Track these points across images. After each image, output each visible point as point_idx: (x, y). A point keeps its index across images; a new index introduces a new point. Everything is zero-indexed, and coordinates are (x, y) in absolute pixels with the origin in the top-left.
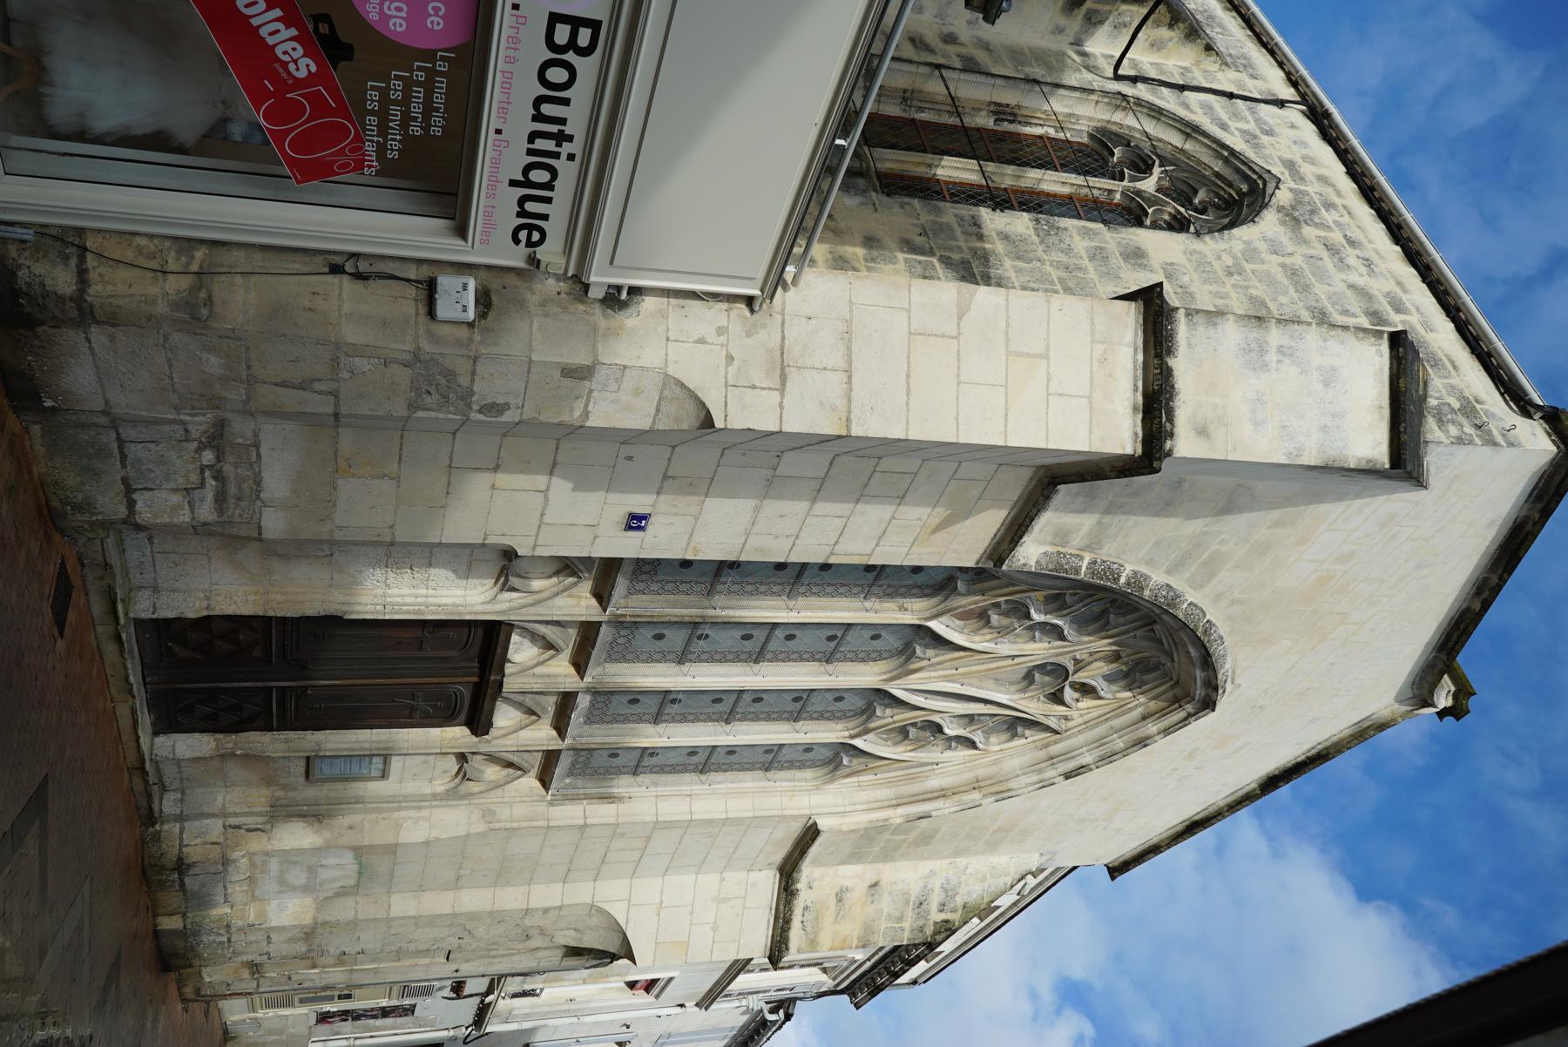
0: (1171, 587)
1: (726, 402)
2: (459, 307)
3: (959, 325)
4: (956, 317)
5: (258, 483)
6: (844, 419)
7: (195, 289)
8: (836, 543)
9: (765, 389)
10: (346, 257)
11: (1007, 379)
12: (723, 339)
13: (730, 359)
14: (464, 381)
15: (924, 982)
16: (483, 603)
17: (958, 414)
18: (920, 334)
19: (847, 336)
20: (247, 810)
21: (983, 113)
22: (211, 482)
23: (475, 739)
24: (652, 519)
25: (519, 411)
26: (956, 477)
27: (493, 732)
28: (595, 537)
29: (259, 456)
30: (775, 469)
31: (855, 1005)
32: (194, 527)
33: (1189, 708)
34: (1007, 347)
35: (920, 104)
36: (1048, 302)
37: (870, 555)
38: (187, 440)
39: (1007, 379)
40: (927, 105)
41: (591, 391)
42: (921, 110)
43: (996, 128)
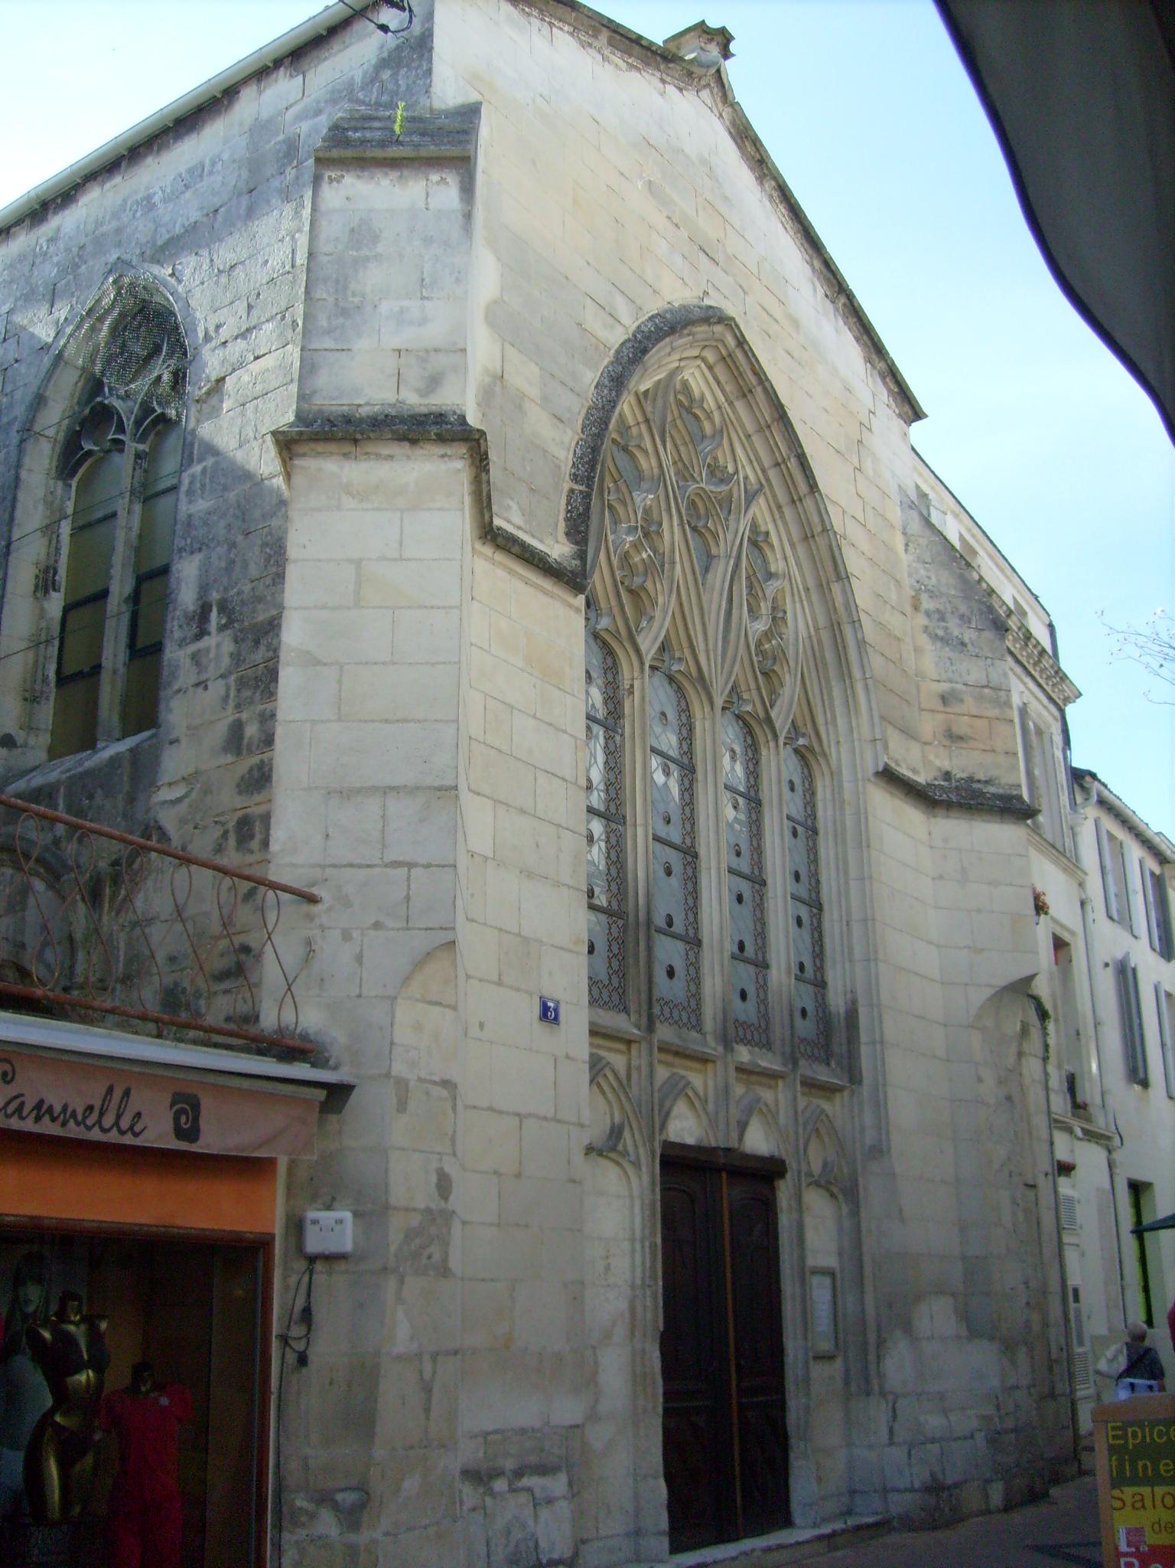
0: (598, 383)
1: (426, 929)
2: (337, 1228)
3: (325, 664)
4: (318, 668)
5: (523, 1431)
6: (439, 794)
7: (336, 1506)
8: (564, 779)
9: (409, 886)
10: (288, 1349)
11: (386, 607)
12: (355, 934)
13: (377, 925)
14: (415, 1220)
15: (1049, 615)
16: (640, 1178)
17: (427, 663)
18: (339, 709)
19: (346, 794)
21: (46, 605)
22: (526, 1481)
23: (788, 1176)
24: (546, 994)
25: (444, 1157)
26: (486, 647)
27: (784, 1157)
28: (568, 1057)
29: (496, 1432)
30: (486, 858)
31: (1077, 697)
32: (573, 1496)
33: (1067, 1550)
34: (349, 608)
35: (39, 681)
36: (296, 561)
37: (576, 738)
38: (484, 1508)
39: (386, 607)
40: (40, 673)
41: (420, 1080)
42: (45, 679)
43: (63, 590)
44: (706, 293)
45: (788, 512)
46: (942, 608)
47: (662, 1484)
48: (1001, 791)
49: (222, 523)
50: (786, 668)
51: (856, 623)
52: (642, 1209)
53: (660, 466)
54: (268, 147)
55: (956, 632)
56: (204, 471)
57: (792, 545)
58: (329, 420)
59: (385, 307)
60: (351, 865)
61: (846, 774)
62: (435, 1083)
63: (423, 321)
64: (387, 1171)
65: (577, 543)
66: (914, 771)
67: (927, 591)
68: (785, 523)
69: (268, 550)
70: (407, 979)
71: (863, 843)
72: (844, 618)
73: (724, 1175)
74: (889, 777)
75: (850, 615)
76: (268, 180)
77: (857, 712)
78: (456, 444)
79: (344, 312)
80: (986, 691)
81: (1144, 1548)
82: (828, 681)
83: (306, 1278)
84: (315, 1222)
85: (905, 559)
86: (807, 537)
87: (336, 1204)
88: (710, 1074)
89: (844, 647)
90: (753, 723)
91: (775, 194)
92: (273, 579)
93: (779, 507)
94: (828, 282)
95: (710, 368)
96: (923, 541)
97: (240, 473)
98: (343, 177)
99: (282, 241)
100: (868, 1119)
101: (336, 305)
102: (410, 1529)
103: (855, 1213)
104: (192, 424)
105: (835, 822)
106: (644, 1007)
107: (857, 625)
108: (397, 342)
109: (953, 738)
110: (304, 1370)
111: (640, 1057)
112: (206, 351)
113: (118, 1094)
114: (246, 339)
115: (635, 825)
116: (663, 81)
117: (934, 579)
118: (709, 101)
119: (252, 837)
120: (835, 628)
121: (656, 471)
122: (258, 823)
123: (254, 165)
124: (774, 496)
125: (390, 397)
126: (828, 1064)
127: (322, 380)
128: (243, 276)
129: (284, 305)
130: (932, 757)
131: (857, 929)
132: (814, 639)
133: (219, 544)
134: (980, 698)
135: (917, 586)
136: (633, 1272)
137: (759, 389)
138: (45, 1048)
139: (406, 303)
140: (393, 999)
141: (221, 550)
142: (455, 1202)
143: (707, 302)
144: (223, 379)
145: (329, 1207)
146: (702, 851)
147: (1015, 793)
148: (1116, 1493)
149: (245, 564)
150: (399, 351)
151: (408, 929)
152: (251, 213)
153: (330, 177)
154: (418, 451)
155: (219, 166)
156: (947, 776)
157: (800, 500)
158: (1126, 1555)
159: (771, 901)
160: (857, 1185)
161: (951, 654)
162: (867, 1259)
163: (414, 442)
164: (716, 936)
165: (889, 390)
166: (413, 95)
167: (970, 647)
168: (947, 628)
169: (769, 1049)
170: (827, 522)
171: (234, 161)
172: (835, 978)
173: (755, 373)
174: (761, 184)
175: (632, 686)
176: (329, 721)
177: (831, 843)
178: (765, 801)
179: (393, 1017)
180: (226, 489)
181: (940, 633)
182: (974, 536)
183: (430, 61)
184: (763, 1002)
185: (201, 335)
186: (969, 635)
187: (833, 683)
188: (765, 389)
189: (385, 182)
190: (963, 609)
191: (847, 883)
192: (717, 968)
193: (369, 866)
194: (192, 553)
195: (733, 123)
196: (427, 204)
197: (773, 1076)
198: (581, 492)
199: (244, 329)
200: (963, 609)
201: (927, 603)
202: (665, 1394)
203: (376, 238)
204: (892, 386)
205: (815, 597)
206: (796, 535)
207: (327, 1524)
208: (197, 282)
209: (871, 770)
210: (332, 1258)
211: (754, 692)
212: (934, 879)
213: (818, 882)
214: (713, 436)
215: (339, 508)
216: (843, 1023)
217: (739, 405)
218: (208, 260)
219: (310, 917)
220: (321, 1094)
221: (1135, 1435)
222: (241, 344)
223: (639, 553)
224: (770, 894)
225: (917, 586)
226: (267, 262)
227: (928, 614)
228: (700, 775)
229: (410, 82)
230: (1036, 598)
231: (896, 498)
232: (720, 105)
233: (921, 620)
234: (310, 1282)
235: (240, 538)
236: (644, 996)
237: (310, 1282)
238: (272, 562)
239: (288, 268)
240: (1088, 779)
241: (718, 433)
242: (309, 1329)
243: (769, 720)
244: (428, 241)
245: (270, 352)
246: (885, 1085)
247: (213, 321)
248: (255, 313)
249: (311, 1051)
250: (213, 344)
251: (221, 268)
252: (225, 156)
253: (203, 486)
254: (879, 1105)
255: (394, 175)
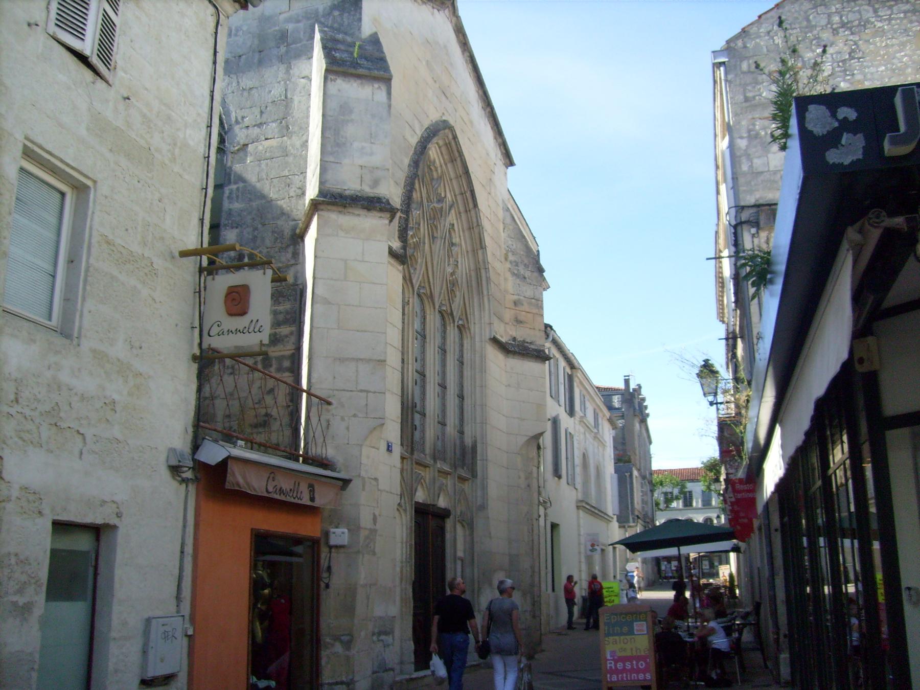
7: (341, 642)
13: (355, 415)
15: (538, 246)
16: (406, 516)
19: (342, 360)
20: (684, 550)
23: (451, 517)
27: (450, 508)
28: (394, 466)
41: (369, 478)
44: (443, 114)
45: (463, 215)
46: (517, 260)
47: (412, 643)
48: (536, 348)
49: (249, 217)
50: (457, 289)
51: (487, 269)
52: (407, 530)
53: (422, 197)
54: (270, 31)
55: (522, 272)
56: (238, 189)
57: (463, 231)
58: (334, 196)
59: (356, 145)
60: (344, 390)
61: (477, 339)
62: (372, 479)
63: (372, 154)
64: (359, 514)
65: (402, 242)
66: (502, 337)
67: (511, 251)
68: (461, 220)
69: (276, 235)
70: (366, 438)
71: (483, 370)
72: (482, 267)
73: (430, 516)
74: (495, 341)
75: (485, 265)
76: (270, 49)
77: (484, 310)
78: (386, 213)
79: (338, 145)
80: (533, 300)
81: (616, 658)
82: (472, 295)
83: (328, 555)
84: (334, 533)
85: (503, 235)
86: (470, 228)
87: (340, 526)
88: (427, 473)
89: (481, 280)
90: (445, 315)
91: (468, 59)
92: (279, 249)
93: (460, 213)
94: (484, 101)
95: (440, 148)
96: (511, 227)
97: (259, 194)
98: (336, 79)
99: (279, 82)
100: (479, 493)
101: (335, 141)
102: (362, 651)
103: (472, 534)
104: (229, 164)
105: (471, 360)
106: (410, 444)
107: (487, 270)
108: (361, 162)
109: (518, 321)
110: (328, 590)
111: (407, 465)
112: (237, 129)
113: (297, 484)
114: (260, 128)
115: (408, 364)
116: (433, 8)
117: (514, 245)
118: (447, 14)
119: (271, 366)
120: (478, 270)
121: (419, 199)
122: (274, 359)
123: (262, 38)
124: (458, 208)
125: (358, 187)
126: (463, 469)
127: (329, 176)
128: (257, 95)
129: (281, 116)
130: (508, 330)
131: (478, 409)
132: (468, 275)
133: (248, 226)
134: (530, 304)
135: (507, 249)
136: (402, 557)
137: (459, 159)
138: (284, 468)
139: (364, 144)
140: (361, 446)
141: (250, 230)
142: (378, 527)
143: (444, 118)
144: (247, 145)
145: (337, 527)
146: (428, 375)
147: (542, 349)
148: (607, 639)
149: (263, 239)
150: (361, 166)
151: (368, 418)
152: (260, 63)
153: (331, 79)
154: (370, 214)
155: (240, 33)
156: (514, 339)
157: (470, 211)
158: (609, 660)
159: (448, 396)
160: (473, 522)
161: (520, 283)
162: (476, 554)
163: (369, 210)
164: (432, 413)
165: (501, 152)
166: (351, 29)
167: (528, 280)
168: (518, 270)
169: (445, 462)
170: (479, 222)
171: (250, 33)
172: (468, 430)
173: (458, 151)
174: (463, 54)
175: (409, 301)
176: (335, 329)
177: (469, 369)
178: (448, 351)
179: (361, 453)
180: (250, 200)
181: (516, 272)
182: (513, 209)
183: (361, 14)
184: (443, 441)
185: (233, 119)
186: (528, 274)
187: (475, 296)
188: (461, 160)
189: (355, 85)
190: (526, 261)
191: (475, 387)
192: (432, 426)
193: (351, 391)
194: (232, 228)
195: (456, 25)
196: (373, 98)
197: (447, 474)
198: (404, 217)
199: (258, 122)
200: (526, 261)
201: (511, 258)
202: (414, 607)
203: (351, 112)
204: (503, 149)
205: (470, 255)
206: (465, 226)
207: (338, 648)
208: (230, 91)
209: (488, 337)
210: (337, 547)
211: (447, 301)
212: (506, 386)
213: (462, 386)
214: (437, 179)
215: (337, 235)
216: (470, 451)
217: (449, 165)
218: (236, 81)
219: (328, 411)
220: (341, 483)
221: (614, 618)
222: (257, 130)
223: (413, 239)
224: (448, 393)
225: (507, 249)
226: (271, 91)
227: (511, 262)
228: (428, 340)
229: (350, 21)
230: (534, 238)
231: (501, 205)
232: (452, 16)
233: (508, 265)
234: (330, 557)
235: (260, 226)
236: (410, 440)
237: (330, 557)
238: (278, 241)
239: (283, 98)
240: (549, 329)
241: (440, 178)
242: (330, 575)
243: (452, 314)
244: (373, 116)
245: (274, 138)
246: (487, 479)
247: (240, 114)
248: (264, 116)
249: (329, 465)
250: (241, 126)
251: (244, 87)
252: (245, 28)
253: (237, 197)
254: (484, 488)
255: (359, 81)
